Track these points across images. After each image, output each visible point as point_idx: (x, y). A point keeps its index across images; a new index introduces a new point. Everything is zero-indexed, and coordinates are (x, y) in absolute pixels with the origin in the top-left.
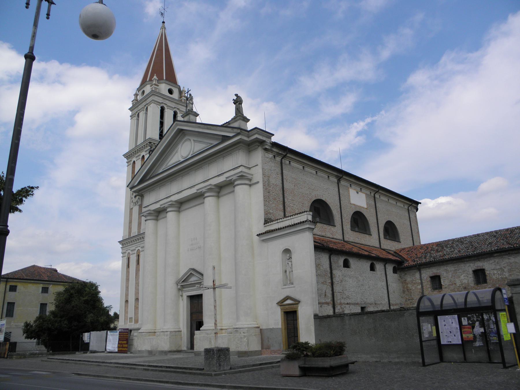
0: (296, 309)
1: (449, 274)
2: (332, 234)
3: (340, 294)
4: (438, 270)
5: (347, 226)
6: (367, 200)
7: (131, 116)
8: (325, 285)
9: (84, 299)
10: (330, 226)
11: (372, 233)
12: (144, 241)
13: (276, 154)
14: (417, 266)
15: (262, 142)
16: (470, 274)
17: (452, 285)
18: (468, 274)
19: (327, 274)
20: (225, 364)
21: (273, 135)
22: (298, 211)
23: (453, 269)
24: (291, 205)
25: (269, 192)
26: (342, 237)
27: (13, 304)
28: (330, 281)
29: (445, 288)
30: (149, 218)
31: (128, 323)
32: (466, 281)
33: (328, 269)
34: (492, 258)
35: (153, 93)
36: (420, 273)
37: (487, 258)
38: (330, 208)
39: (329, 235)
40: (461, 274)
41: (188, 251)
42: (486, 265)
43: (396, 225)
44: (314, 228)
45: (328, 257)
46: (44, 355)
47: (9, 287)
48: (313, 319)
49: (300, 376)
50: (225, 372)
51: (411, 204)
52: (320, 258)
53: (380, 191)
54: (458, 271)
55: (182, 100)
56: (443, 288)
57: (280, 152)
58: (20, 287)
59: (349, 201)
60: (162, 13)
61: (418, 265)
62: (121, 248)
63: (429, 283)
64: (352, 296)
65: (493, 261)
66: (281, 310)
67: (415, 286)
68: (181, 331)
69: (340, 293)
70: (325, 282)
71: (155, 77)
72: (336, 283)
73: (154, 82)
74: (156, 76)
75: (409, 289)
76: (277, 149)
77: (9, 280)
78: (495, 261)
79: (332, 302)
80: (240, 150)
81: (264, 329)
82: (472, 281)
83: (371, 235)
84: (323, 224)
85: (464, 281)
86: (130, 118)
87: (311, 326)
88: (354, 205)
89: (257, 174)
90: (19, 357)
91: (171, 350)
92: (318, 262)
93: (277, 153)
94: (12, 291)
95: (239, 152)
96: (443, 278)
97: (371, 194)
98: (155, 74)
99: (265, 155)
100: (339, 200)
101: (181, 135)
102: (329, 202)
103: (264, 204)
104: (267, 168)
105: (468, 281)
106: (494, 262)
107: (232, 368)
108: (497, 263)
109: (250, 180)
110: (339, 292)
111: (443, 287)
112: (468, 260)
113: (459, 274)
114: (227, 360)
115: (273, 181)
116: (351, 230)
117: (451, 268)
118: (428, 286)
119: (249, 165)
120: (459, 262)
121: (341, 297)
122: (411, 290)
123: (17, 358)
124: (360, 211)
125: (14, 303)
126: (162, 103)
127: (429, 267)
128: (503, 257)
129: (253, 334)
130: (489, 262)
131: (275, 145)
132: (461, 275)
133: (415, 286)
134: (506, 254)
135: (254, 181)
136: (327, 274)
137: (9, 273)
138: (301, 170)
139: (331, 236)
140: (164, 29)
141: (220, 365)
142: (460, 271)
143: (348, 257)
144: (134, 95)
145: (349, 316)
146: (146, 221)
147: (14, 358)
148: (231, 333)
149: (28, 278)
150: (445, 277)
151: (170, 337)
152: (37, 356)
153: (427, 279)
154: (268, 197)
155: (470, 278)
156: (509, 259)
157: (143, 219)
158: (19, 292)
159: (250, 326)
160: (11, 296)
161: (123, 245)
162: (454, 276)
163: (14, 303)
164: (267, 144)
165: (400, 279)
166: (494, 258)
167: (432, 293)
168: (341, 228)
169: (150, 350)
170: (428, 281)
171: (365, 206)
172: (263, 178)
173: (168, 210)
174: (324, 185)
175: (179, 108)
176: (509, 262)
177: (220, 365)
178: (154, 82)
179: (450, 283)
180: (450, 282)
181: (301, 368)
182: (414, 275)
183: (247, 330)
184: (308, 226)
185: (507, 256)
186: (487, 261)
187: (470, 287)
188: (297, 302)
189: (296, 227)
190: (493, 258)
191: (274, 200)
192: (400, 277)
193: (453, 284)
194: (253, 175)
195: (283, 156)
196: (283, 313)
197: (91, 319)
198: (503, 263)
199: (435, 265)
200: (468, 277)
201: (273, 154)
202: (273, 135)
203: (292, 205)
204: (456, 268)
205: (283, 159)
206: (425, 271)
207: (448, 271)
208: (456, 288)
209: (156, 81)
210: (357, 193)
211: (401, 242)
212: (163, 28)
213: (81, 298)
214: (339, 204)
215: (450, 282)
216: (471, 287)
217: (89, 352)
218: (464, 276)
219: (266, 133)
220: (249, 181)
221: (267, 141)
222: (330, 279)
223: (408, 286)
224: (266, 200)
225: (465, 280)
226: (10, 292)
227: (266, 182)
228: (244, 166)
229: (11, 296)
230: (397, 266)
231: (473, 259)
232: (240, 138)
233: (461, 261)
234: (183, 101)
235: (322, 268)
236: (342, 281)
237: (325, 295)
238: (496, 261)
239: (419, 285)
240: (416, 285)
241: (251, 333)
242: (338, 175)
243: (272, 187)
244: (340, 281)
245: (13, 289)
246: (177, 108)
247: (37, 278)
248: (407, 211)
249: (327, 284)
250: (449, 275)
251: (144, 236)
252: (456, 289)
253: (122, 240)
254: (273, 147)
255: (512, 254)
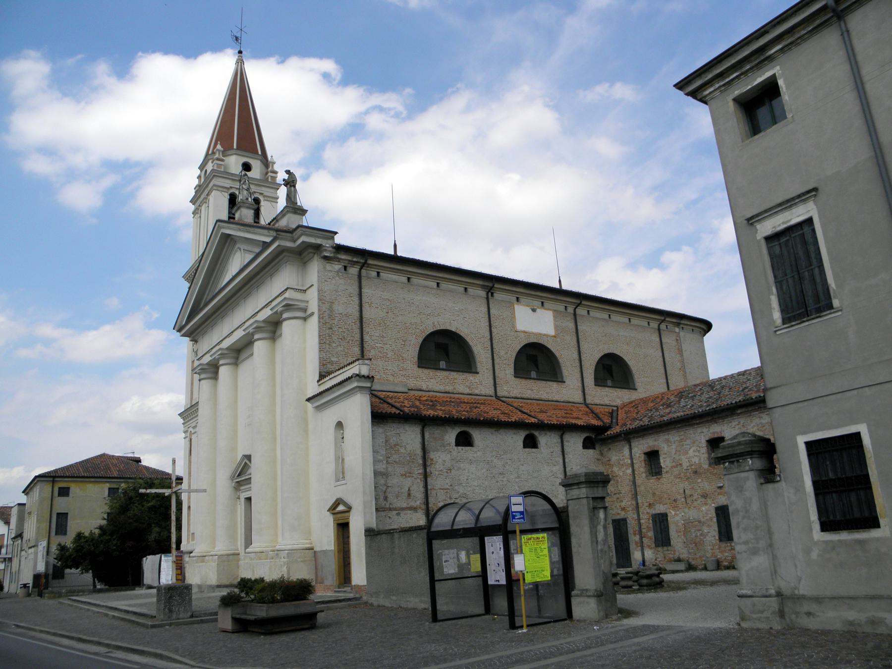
0: (346, 520)
1: (671, 447)
2: (469, 388)
3: (445, 491)
4: (655, 441)
5: (506, 371)
6: (555, 320)
7: (193, 213)
8: (409, 479)
9: (150, 504)
10: (464, 374)
11: (565, 379)
12: (197, 416)
13: (349, 264)
14: (623, 435)
15: (318, 248)
16: (702, 447)
17: (676, 466)
18: (700, 447)
19: (414, 459)
20: (180, 609)
21: (336, 233)
22: (393, 354)
23: (677, 438)
24: (377, 345)
25: (332, 329)
26: (493, 391)
27: (65, 515)
28: (421, 471)
29: (667, 472)
30: (203, 376)
31: (191, 542)
32: (696, 460)
33: (419, 452)
34: (735, 418)
35: (213, 174)
36: (630, 446)
37: (727, 416)
38: (468, 343)
39: (462, 388)
40: (688, 446)
41: (245, 426)
42: (727, 429)
43: (627, 360)
44: (370, 386)
45: (419, 431)
46: (86, 593)
47: (57, 490)
48: (364, 537)
49: (235, 631)
50: (171, 621)
51: (663, 318)
52: (399, 434)
53: (584, 302)
54: (685, 441)
55: (268, 178)
56: (663, 472)
57: (355, 260)
58: (76, 489)
59: (514, 326)
60: (237, 39)
61: (624, 434)
62: (183, 424)
63: (643, 464)
64: (474, 494)
65: (737, 423)
66: (334, 520)
67: (623, 470)
68: (239, 555)
69: (445, 489)
70: (410, 473)
71: (219, 147)
72: (437, 473)
73: (217, 156)
74: (220, 144)
75: (614, 475)
76: (348, 255)
77: (56, 479)
78: (739, 422)
79: (424, 507)
80: (288, 263)
81: (318, 551)
82: (706, 459)
83: (565, 382)
84: (450, 372)
85: (693, 460)
86: (193, 216)
87: (362, 549)
88: (525, 332)
89: (312, 300)
90: (52, 595)
91: (219, 584)
92: (393, 440)
93: (349, 261)
94: (63, 496)
95: (286, 266)
96: (664, 454)
97: (566, 310)
98: (219, 142)
99: (324, 268)
100: (488, 328)
101: (230, 243)
102: (464, 331)
103: (320, 348)
104: (328, 288)
105: (700, 459)
106: (738, 425)
107: (194, 616)
108: (743, 426)
109: (305, 310)
110: (443, 489)
111: (664, 471)
112: (698, 422)
113: (686, 448)
114: (186, 604)
115: (339, 308)
116: (515, 377)
117: (674, 437)
118: (642, 470)
119: (303, 286)
120: (686, 425)
121: (447, 497)
122: (617, 476)
123: (50, 598)
124: (540, 342)
125: (67, 514)
126: (231, 187)
127: (643, 436)
128: (752, 414)
129: (299, 560)
130: (730, 424)
131: (340, 248)
132: (690, 449)
133: (623, 470)
134: (748, 411)
135: (309, 312)
136: (414, 459)
137: (59, 468)
138: (405, 284)
139: (467, 391)
140: (240, 63)
141: (171, 611)
142: (688, 442)
143: (469, 427)
144: (198, 178)
145: (398, 533)
146: (200, 380)
147: (46, 598)
148: (272, 559)
149: (86, 475)
150: (666, 452)
151: (217, 564)
152: (77, 594)
153: (639, 457)
154: (330, 336)
155: (703, 454)
156: (760, 418)
157: (197, 377)
158: (73, 497)
159: (295, 547)
160: (61, 505)
161: (184, 419)
162: (680, 451)
163: (67, 514)
164: (326, 250)
165: (599, 457)
166: (739, 417)
167: (648, 482)
168: (492, 376)
169: (199, 583)
170: (642, 461)
171: (552, 332)
172: (319, 306)
173: (221, 362)
174: (454, 304)
175: (262, 192)
176: (761, 423)
177: (171, 611)
178: (217, 156)
179: (674, 464)
180: (674, 461)
181: (235, 620)
182: (622, 450)
183: (288, 553)
184: (355, 384)
185: (757, 413)
186: (728, 422)
187: (703, 470)
188: (349, 508)
189: (345, 386)
190: (737, 417)
191: (340, 340)
192: (602, 454)
193: (677, 465)
194: (308, 301)
195: (361, 264)
196: (336, 525)
197: (156, 536)
198: (752, 425)
199: (651, 432)
200: (699, 451)
201: (343, 264)
202: (336, 233)
203: (380, 345)
204: (682, 437)
205: (362, 270)
206: (637, 443)
207: (671, 443)
208: (683, 473)
209: (219, 153)
210: (534, 310)
211: (636, 390)
212: (238, 63)
213: (145, 503)
214: (487, 334)
215: (674, 461)
216: (705, 470)
217: (144, 588)
218: (694, 451)
219: (321, 233)
220: (303, 312)
221: (323, 245)
222: (422, 467)
223: (613, 469)
224: (324, 341)
225: (695, 458)
226: (60, 498)
227: (325, 312)
228: (294, 289)
229: (61, 505)
230: (595, 436)
231: (705, 419)
232: (279, 246)
233: (687, 424)
234: (270, 180)
235: (402, 450)
236: (450, 470)
237: (409, 495)
238: (742, 423)
239: (629, 469)
240: (624, 468)
241: (295, 558)
242: (486, 284)
243: (337, 318)
244: (445, 470)
245: (64, 492)
246: (258, 193)
247: (102, 473)
248: (657, 331)
249: (414, 476)
250: (672, 449)
251: (197, 408)
252: (682, 474)
253: (185, 410)
254: (339, 253)
255: (765, 409)
